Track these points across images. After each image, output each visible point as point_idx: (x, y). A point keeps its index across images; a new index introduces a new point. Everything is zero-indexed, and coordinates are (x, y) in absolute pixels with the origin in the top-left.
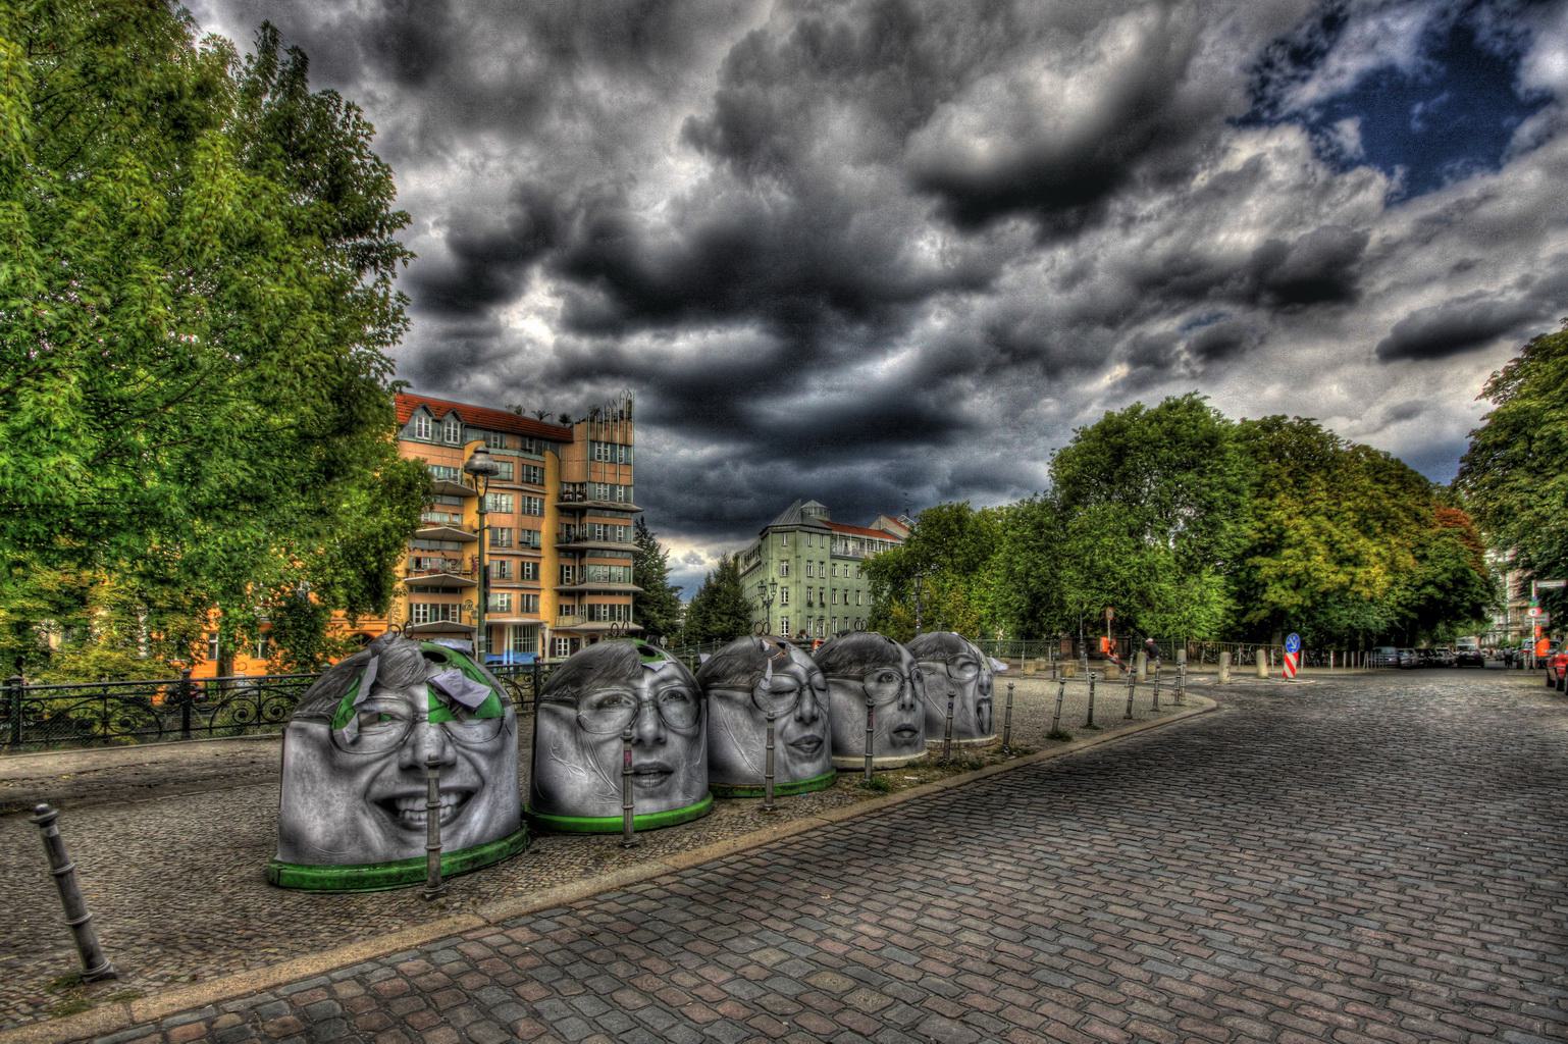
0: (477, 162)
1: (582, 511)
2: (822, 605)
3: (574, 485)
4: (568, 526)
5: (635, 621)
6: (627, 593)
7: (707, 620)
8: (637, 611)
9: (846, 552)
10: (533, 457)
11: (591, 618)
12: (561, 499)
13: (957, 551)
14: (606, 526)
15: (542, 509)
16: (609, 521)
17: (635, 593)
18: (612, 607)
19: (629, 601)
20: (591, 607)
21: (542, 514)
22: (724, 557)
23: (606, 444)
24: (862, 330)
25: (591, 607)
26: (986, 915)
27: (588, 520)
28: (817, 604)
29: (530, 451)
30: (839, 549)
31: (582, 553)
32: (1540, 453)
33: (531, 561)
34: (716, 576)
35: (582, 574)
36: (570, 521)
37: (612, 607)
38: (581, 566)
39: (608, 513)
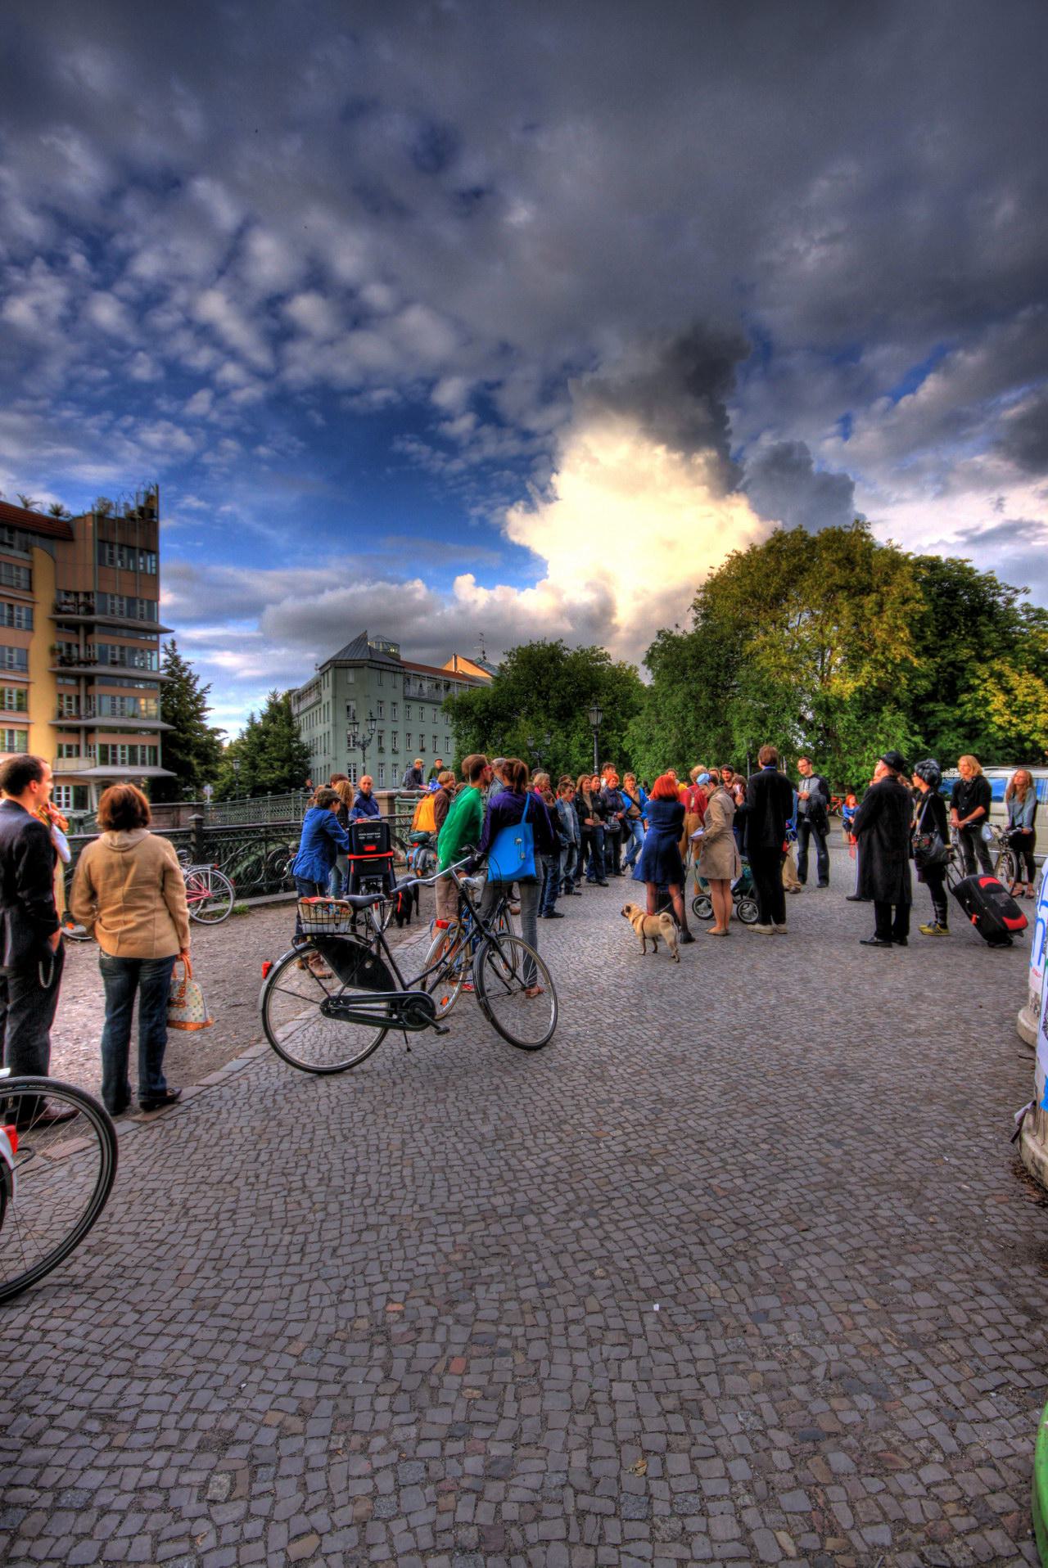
0: (893, 706)
1: (89, 628)
2: (395, 752)
3: (77, 594)
4: (69, 646)
5: (164, 766)
6: (154, 732)
7: (254, 766)
8: (166, 754)
9: (421, 692)
10: (13, 552)
11: (104, 761)
12: (58, 610)
13: (552, 693)
14: (122, 648)
15: (31, 620)
16: (129, 643)
17: (164, 733)
18: (133, 749)
19: (157, 741)
20: (104, 748)
21: (31, 629)
22: (274, 695)
23: (122, 546)
24: (507, 499)
25: (104, 748)
26: (479, 1217)
27: (98, 639)
28: (388, 750)
29: (11, 546)
30: (413, 690)
31: (90, 680)
32: (808, 679)
33: (16, 688)
34: (264, 717)
35: (89, 707)
36: (72, 639)
37: (133, 749)
38: (88, 697)
39: (125, 633)
